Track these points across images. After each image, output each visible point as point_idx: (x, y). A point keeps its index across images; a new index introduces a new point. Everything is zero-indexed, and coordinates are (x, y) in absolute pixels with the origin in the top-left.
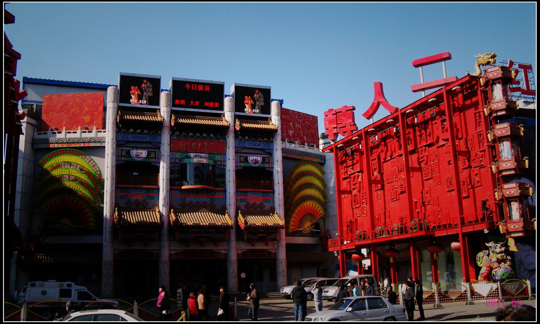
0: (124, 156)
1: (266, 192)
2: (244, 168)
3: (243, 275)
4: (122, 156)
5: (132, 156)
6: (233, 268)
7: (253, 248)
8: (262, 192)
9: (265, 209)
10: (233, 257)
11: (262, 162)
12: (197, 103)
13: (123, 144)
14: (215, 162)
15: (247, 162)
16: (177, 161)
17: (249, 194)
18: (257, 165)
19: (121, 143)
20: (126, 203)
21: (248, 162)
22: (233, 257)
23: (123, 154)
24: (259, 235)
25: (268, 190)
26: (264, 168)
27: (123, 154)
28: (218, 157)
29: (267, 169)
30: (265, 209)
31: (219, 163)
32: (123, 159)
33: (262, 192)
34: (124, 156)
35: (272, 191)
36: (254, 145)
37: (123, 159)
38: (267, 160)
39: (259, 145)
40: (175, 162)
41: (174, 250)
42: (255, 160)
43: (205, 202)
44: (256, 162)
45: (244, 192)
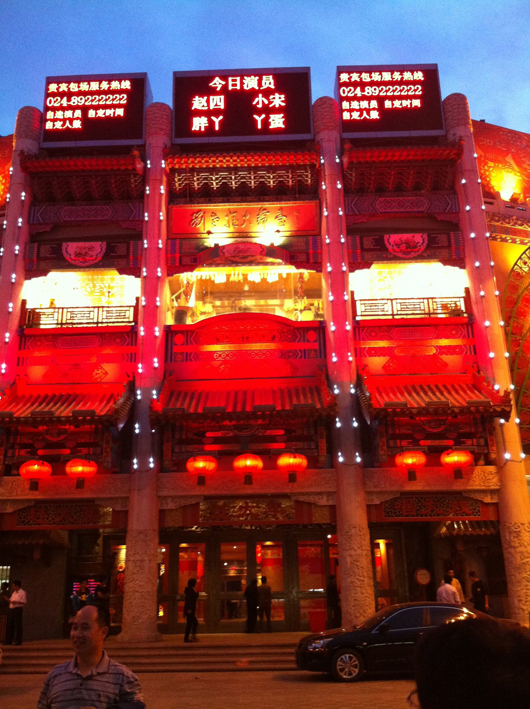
41: (173, 498)
42: (407, 242)
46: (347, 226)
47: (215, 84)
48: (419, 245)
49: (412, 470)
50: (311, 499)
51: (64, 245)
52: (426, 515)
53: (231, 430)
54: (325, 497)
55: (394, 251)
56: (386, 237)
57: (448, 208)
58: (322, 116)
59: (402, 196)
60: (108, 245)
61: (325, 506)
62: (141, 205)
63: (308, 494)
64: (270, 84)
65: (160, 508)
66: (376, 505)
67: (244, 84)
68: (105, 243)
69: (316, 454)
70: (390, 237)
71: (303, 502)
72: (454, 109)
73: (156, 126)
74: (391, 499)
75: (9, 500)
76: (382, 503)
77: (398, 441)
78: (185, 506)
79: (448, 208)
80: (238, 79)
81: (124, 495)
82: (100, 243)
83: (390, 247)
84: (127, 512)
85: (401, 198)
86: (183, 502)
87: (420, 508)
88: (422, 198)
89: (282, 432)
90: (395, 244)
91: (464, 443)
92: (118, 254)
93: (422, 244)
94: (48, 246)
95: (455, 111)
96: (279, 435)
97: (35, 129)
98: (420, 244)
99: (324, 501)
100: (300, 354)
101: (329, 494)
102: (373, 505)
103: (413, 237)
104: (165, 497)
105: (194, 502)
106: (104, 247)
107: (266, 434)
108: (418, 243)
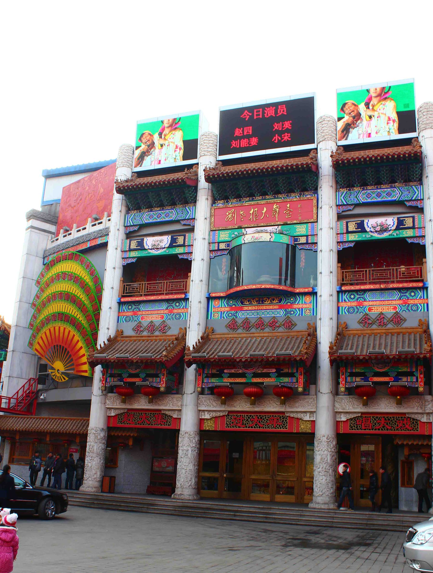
0: (135, 250)
1: (408, 289)
2: (140, 259)
3: (341, 469)
4: (130, 250)
5: (146, 247)
6: (323, 452)
7: (257, 409)
8: (399, 289)
9: (406, 325)
10: (324, 430)
11: (397, 228)
12: (254, 141)
13: (135, 231)
14: (295, 238)
15: (364, 231)
16: (222, 246)
17: (368, 296)
18: (385, 235)
19: (132, 229)
20: (360, 323)
21: (366, 231)
22: (188, 425)
23: (350, 229)
24: (376, 379)
25: (415, 285)
26: (176, 256)
27: (350, 229)
28: (301, 230)
29: (409, 241)
30: (406, 325)
31: (303, 240)
32: (133, 254)
33: (399, 289)
34: (135, 250)
35: (421, 285)
36: (379, 195)
37: (133, 254)
38: (409, 222)
39: (389, 194)
40: (219, 250)
41: (209, 411)
42: (382, 225)
43: (247, 318)
44: (384, 229)
45: (357, 291)
46: (337, 214)
47: (245, 115)
48: (390, 226)
49: (281, 405)
50: (299, 416)
51: (145, 239)
52: (379, 429)
53: (241, 368)
54: (308, 414)
55: (371, 232)
56: (366, 221)
57: (415, 196)
58: (322, 131)
59: (380, 189)
60: (172, 237)
61: (309, 421)
62: (194, 207)
63: (297, 412)
64: (283, 111)
65: (201, 418)
66: (343, 421)
67: (265, 113)
68: (170, 236)
69: (297, 386)
70: (368, 221)
71: (293, 417)
72: (424, 115)
73: (205, 150)
74: (354, 417)
75: (112, 408)
76: (348, 420)
77: (354, 378)
78: (216, 417)
79: (415, 196)
80: (241, 146)
81: (177, 408)
82: (167, 236)
83: (368, 229)
84: (180, 419)
85: (379, 190)
86: (214, 414)
87: (375, 424)
88: (395, 189)
89: (274, 370)
90: (372, 227)
91: (400, 379)
92: (178, 244)
93: (393, 226)
94: (136, 241)
95: (425, 117)
96: (272, 373)
97: (129, 159)
98: (391, 226)
99: (307, 417)
100: (299, 312)
101: (312, 413)
102: (341, 421)
103: (386, 220)
104: (204, 411)
105: (221, 415)
106: (170, 240)
107: (264, 372)
108: (390, 225)
